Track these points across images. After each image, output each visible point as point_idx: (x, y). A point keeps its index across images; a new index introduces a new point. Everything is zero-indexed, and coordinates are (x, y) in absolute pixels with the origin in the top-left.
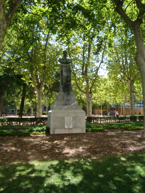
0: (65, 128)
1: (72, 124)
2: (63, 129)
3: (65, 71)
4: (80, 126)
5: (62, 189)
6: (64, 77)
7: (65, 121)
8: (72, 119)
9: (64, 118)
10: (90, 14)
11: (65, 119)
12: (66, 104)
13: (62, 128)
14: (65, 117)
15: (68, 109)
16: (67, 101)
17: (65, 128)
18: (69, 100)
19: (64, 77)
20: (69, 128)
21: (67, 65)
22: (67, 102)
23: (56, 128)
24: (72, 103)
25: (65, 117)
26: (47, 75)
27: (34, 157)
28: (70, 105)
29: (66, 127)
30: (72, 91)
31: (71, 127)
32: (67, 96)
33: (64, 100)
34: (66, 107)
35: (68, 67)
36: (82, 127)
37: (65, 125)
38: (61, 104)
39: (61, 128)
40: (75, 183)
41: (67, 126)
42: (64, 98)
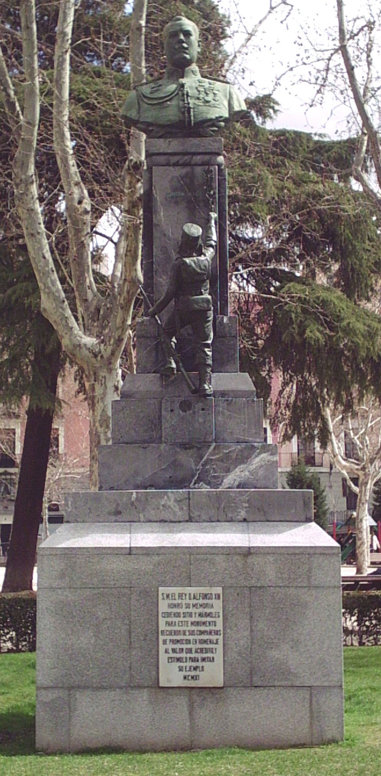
0: (163, 683)
1: (219, 656)
2: (145, 694)
6: (165, 250)
7: (162, 626)
8: (217, 606)
11: (163, 606)
12: (180, 474)
13: (139, 687)
16: (185, 446)
17: (163, 683)
19: (165, 250)
21: (193, 144)
22: (187, 459)
23: (86, 688)
28: (215, 483)
29: (171, 675)
30: (249, 96)
31: (213, 674)
34: (171, 496)
35: (198, 159)
37: (163, 657)
40: (221, 11)
42: (156, 423)
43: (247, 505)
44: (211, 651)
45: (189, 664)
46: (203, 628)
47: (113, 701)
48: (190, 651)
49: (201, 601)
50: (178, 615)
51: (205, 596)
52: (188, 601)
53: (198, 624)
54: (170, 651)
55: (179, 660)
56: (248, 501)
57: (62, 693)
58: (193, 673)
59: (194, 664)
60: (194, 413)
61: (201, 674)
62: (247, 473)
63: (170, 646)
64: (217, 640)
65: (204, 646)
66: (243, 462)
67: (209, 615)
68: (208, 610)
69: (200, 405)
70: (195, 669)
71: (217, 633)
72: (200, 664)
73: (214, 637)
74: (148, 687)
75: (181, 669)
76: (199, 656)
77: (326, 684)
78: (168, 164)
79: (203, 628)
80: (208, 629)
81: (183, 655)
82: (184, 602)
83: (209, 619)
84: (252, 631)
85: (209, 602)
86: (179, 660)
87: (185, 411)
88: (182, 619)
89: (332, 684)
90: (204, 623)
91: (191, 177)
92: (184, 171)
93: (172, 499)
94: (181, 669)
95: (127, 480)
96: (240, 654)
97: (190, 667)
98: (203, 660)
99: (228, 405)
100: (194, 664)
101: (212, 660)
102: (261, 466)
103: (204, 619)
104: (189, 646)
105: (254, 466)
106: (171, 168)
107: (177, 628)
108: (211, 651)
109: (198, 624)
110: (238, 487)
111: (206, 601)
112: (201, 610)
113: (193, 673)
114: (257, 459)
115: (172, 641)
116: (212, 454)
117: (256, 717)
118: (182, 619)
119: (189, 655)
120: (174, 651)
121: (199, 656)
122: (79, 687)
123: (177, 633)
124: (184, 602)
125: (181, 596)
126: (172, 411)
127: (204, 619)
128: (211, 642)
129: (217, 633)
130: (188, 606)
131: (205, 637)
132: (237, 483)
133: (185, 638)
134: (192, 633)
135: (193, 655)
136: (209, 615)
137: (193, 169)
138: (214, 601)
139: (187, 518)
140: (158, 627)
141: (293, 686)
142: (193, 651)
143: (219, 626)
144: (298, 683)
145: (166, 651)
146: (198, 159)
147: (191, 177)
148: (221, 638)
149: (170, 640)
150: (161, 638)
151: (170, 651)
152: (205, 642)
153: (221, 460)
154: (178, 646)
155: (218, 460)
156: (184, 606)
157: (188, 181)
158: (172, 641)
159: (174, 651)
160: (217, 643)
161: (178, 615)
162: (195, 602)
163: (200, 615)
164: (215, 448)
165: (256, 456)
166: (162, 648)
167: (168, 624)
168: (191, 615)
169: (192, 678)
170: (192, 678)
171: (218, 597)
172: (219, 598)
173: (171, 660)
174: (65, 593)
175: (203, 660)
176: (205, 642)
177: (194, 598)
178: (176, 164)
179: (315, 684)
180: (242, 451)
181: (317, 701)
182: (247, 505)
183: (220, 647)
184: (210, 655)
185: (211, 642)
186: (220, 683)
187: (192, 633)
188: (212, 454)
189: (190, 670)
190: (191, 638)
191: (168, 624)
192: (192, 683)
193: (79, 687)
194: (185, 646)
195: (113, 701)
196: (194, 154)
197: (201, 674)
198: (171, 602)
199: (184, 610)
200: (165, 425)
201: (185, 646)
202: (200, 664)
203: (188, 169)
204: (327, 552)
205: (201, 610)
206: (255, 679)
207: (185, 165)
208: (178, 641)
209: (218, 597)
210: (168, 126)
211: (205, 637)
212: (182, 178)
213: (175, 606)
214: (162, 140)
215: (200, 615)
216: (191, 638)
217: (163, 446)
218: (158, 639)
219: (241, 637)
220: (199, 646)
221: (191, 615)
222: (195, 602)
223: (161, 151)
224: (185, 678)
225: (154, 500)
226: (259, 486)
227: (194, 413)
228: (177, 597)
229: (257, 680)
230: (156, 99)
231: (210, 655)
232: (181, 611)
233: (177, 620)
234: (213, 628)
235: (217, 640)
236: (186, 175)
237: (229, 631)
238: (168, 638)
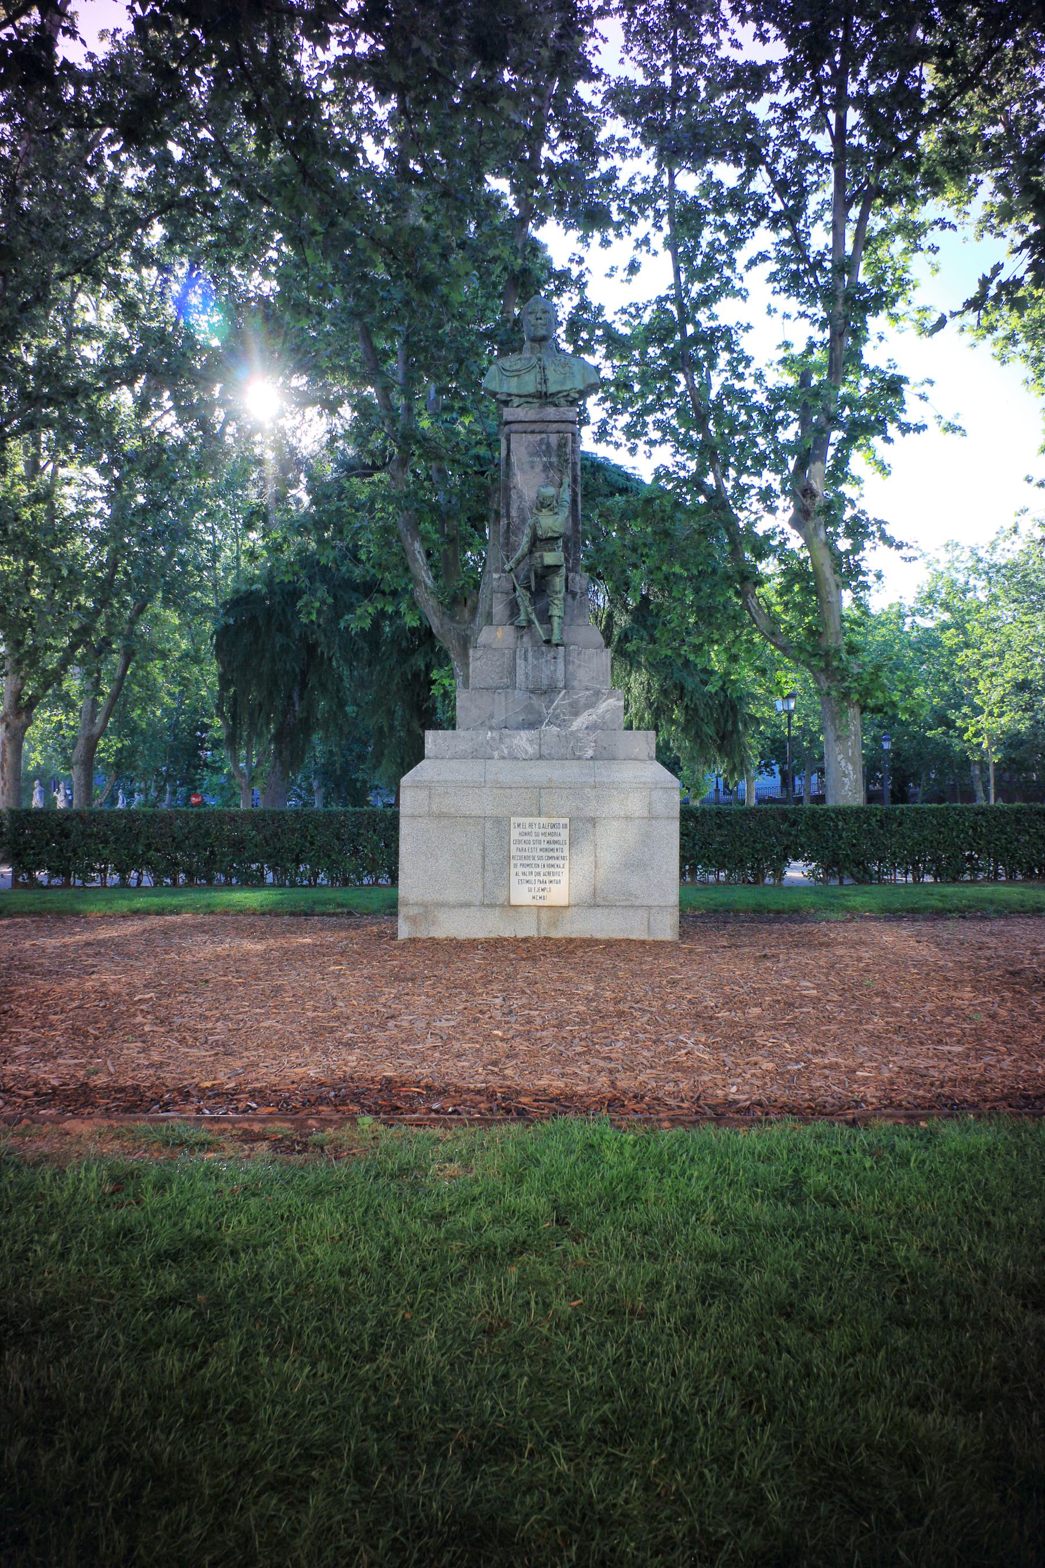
7: (513, 852)
11: (515, 834)
15: (541, 757)
17: (513, 902)
33: (513, 686)
38: (494, 722)
51: (553, 826)
63: (521, 870)
101: (558, 882)
121: (547, 878)
154: (527, 870)
166: (513, 871)
171: (565, 826)
173: (520, 882)
183: (566, 871)
186: (565, 903)
187: (540, 858)
192: (541, 903)
209: (565, 826)
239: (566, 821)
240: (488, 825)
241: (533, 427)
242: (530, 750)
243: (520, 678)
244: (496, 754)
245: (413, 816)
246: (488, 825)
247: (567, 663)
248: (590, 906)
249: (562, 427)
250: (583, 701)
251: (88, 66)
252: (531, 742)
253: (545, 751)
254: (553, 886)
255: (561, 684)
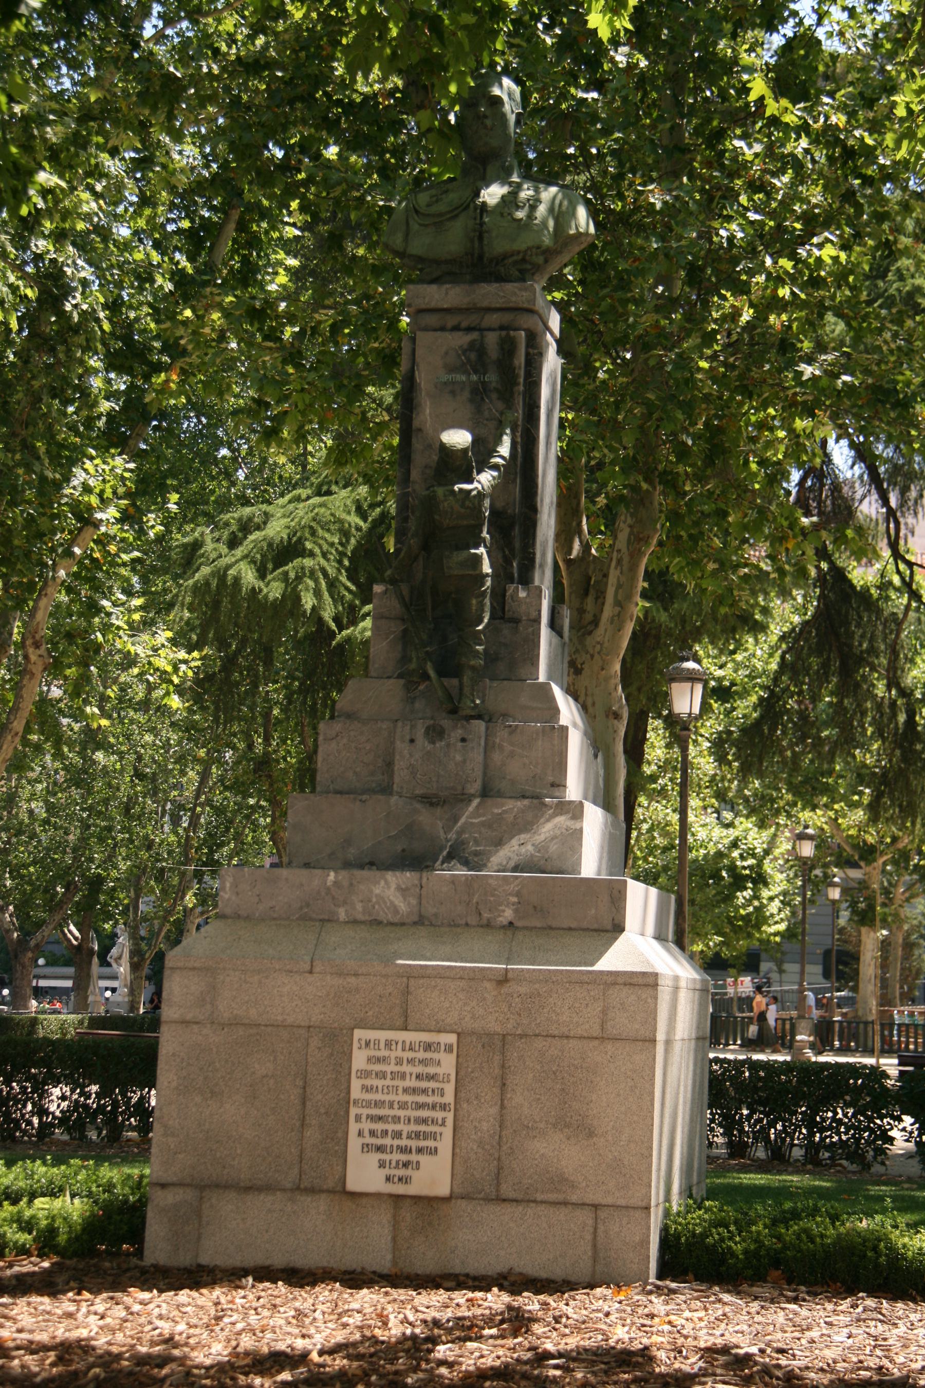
1: (445, 1145)
2: (322, 1203)
3: (452, 389)
4: (560, 1181)
5: (826, 1387)
7: (356, 1092)
8: (448, 1064)
9: (337, 1043)
10: (628, 356)
11: (359, 1060)
13: (312, 1191)
14: (358, 1034)
15: (421, 921)
16: (431, 801)
17: (352, 1185)
18: (463, 799)
20: (397, 1199)
21: (489, 293)
22: (426, 818)
23: (226, 1187)
24: (499, 843)
25: (358, 1034)
26: (20, 1129)
27: (37, 463)
29: (365, 1174)
31: (434, 1176)
32: (435, 733)
33: (386, 790)
34: (390, 890)
36: (591, 1198)
37: (354, 1144)
38: (352, 853)
39: (298, 1189)
41: (374, 1158)
43: (515, 899)
44: (434, 1136)
45: (397, 1156)
46: (422, 1099)
47: (269, 1211)
48: (398, 1135)
49: (421, 1055)
50: (382, 1075)
51: (428, 1047)
52: (399, 1053)
53: (414, 1091)
54: (366, 1133)
55: (380, 1149)
56: (518, 894)
57: (188, 1195)
58: (401, 1172)
59: (404, 1158)
60: (448, 745)
61: (415, 1175)
62: (530, 847)
63: (367, 1126)
64: (444, 1120)
65: (422, 1128)
66: (520, 832)
67: (432, 1077)
68: (431, 1070)
69: (459, 732)
70: (406, 1165)
71: (444, 1107)
72: (414, 1157)
73: (439, 1115)
74: (329, 1191)
75: (382, 1165)
76: (413, 1144)
77: (622, 1202)
78: (443, 329)
79: (422, 1099)
80: (430, 1100)
81: (388, 1141)
82: (393, 1055)
83: (432, 1085)
84: (503, 1107)
85: (435, 1056)
86: (380, 1149)
87: (433, 743)
88: (388, 1082)
89: (632, 1202)
90: (424, 1091)
91: (478, 349)
92: (464, 339)
93: (393, 886)
94: (382, 1165)
95: (333, 853)
96: (481, 1144)
97: (398, 1162)
98: (420, 1150)
99: (511, 733)
100: (404, 1158)
101: (434, 1152)
102: (553, 838)
103: (424, 1084)
104: (397, 1127)
105: (542, 837)
106: (447, 334)
107: (379, 1097)
108: (434, 1136)
109: (414, 1091)
110: (515, 869)
111: (428, 1055)
112: (420, 1069)
113: (401, 1172)
114: (549, 826)
115: (372, 1118)
116: (473, 816)
117: (502, 1253)
118: (388, 1082)
119: (396, 1142)
120: (372, 1133)
121: (413, 1144)
122: (217, 1186)
123: (378, 1104)
124: (393, 1055)
125: (388, 1044)
126: (412, 741)
127: (424, 1084)
128: (434, 1122)
129: (444, 1107)
130: (399, 1062)
131: (424, 1113)
132: (512, 864)
133: (392, 1113)
134: (403, 1106)
135: (404, 1142)
136: (432, 1077)
137: (482, 337)
138: (441, 1056)
139: (416, 919)
140: (349, 1092)
141: (565, 1203)
142: (404, 1135)
143: (449, 1098)
144: (574, 1198)
145: (360, 1134)
146: (493, 319)
147: (478, 349)
148: (450, 1116)
149: (368, 1116)
150: (353, 1111)
151: (366, 1133)
152: (424, 1121)
153: (488, 825)
154: (379, 1127)
155: (482, 824)
156: (393, 1061)
157: (473, 356)
158: (372, 1118)
159: (372, 1133)
160: (443, 1124)
161: (382, 1075)
162: (411, 1055)
163: (418, 1077)
164: (478, 807)
165: (548, 820)
166: (353, 1127)
167: (366, 1089)
168: (403, 1076)
169: (400, 1179)
170: (400, 1179)
171: (449, 1049)
172: (451, 1051)
173: (366, 1148)
174: (205, 1031)
175: (420, 1150)
176: (424, 1121)
177: (411, 1049)
178: (456, 328)
179: (604, 1202)
180: (523, 811)
181: (606, 1232)
182: (515, 899)
183: (448, 1132)
184: (430, 1143)
185: (434, 1122)
186: (444, 1190)
187: (403, 1106)
188: (473, 816)
189: (397, 1167)
190: (402, 1113)
191: (366, 1089)
192: (400, 1189)
193: (217, 1186)
194: (391, 1127)
195: (269, 1211)
196: (489, 310)
197: (415, 1175)
198: (372, 1053)
199: (392, 1068)
200: (400, 765)
201: (391, 1127)
202: (414, 1157)
203: (475, 335)
204: (635, 980)
205: (420, 1069)
206: (504, 1187)
207: (469, 329)
208: (380, 1118)
209: (449, 1049)
210: (447, 262)
211: (424, 1113)
212: (464, 352)
213: (379, 1060)
214: (434, 287)
215: (418, 1077)
216: (402, 1113)
217: (394, 799)
218: (347, 1112)
219: (484, 1116)
220: (413, 1127)
221: (403, 1076)
222: (411, 1055)
223: (433, 305)
224: (388, 1179)
225: (362, 887)
226: (549, 868)
227: (448, 745)
228: (382, 1045)
229: (507, 1190)
230: (433, 215)
231: (430, 1143)
232: (389, 1068)
233: (380, 1083)
234: (437, 1099)
235: (444, 1120)
236: (472, 344)
237: (465, 1106)
238: (365, 1112)
239: (452, 1038)
240: (315, 1042)
241: (451, 321)
242: (402, 906)
243: (401, 773)
244: (342, 914)
245: (185, 1022)
246: (315, 1042)
247: (488, 749)
248: (488, 1200)
249: (506, 318)
250: (510, 817)
251: (873, 491)
252: (403, 891)
253: (430, 910)
254: (423, 1159)
255: (475, 787)
